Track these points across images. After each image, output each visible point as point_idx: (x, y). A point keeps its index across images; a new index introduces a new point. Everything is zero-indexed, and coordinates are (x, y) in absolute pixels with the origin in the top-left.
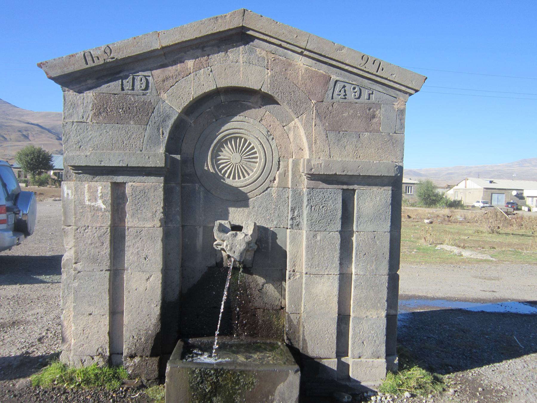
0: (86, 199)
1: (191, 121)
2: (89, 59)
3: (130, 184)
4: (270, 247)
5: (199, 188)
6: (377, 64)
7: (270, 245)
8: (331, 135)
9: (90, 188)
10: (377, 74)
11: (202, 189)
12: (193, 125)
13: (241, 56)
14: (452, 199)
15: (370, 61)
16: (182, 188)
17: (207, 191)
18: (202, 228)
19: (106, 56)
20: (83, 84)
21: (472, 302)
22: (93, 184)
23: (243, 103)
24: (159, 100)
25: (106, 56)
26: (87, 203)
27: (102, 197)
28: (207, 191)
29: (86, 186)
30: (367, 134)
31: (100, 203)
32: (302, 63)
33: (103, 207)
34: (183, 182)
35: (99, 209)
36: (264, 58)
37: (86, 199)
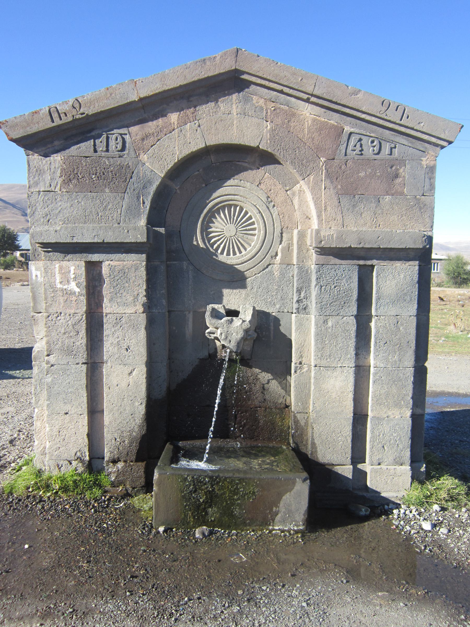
0: (58, 281)
2: (55, 115)
3: (107, 263)
8: (345, 201)
9: (61, 268)
10: (402, 122)
11: (191, 267)
12: (178, 191)
13: (234, 106)
15: (393, 107)
19: (74, 112)
22: (65, 263)
23: (238, 163)
25: (74, 112)
26: (59, 286)
29: (57, 266)
30: (388, 198)
31: (73, 286)
32: (308, 112)
34: (168, 259)
35: (72, 293)
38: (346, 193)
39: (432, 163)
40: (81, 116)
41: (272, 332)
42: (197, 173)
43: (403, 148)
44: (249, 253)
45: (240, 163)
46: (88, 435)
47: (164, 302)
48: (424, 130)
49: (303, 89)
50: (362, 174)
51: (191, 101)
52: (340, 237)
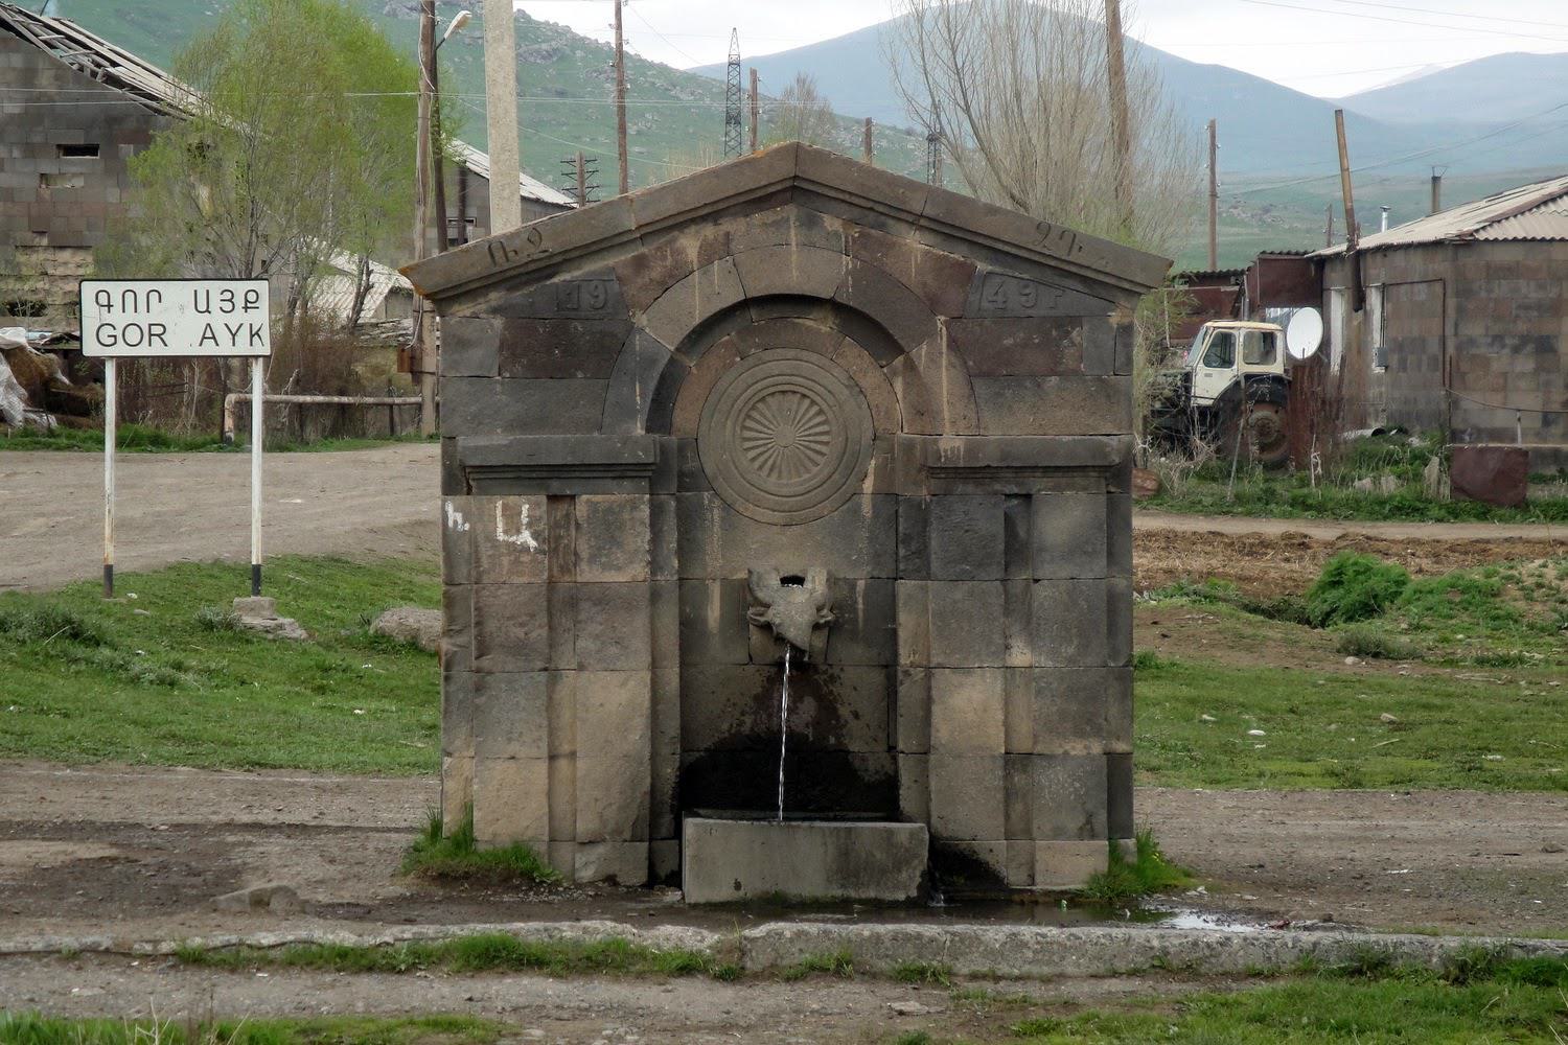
0: (500, 529)
1: (691, 363)
2: (499, 255)
3: (585, 497)
4: (860, 620)
5: (710, 501)
6: (1068, 239)
7: (861, 614)
8: (982, 388)
9: (505, 507)
10: (1070, 258)
11: (717, 502)
12: (694, 371)
13: (793, 232)
14: (429, 723)
15: (1053, 235)
16: (678, 501)
17: (728, 507)
18: (718, 583)
19: (532, 249)
20: (481, 300)
21: (603, 249)
22: (512, 499)
23: (797, 320)
24: (631, 329)
25: (532, 249)
26: (501, 537)
27: (529, 525)
28: (728, 507)
29: (499, 504)
30: (1054, 380)
31: (526, 538)
32: (915, 243)
33: (533, 543)
34: (681, 488)
35: (525, 549)
36: (836, 233)
37: (500, 529)
38: (987, 375)
39: (1126, 321)
40: (542, 255)
41: (861, 614)
42: (727, 338)
43: (1074, 299)
44: (814, 477)
45: (800, 321)
46: (989, 467)
47: (676, 563)
48: (1107, 270)
49: (908, 208)
50: (1008, 342)
51: (920, 471)
52: (971, 450)
